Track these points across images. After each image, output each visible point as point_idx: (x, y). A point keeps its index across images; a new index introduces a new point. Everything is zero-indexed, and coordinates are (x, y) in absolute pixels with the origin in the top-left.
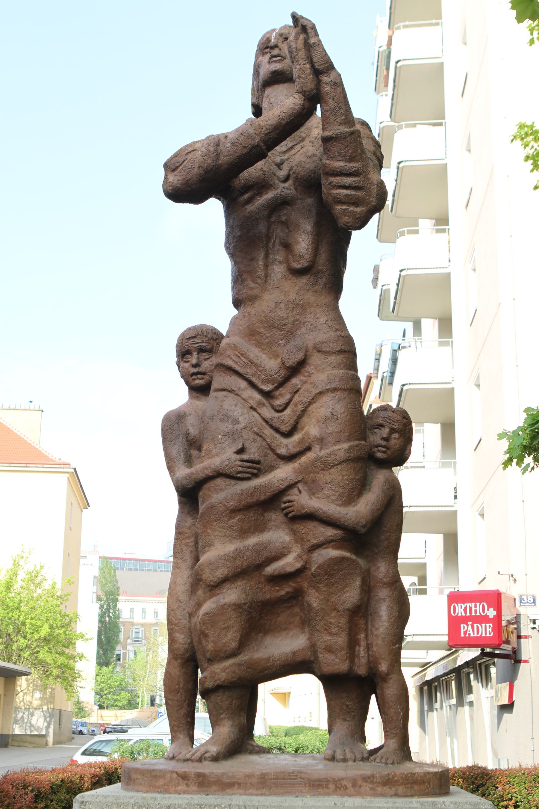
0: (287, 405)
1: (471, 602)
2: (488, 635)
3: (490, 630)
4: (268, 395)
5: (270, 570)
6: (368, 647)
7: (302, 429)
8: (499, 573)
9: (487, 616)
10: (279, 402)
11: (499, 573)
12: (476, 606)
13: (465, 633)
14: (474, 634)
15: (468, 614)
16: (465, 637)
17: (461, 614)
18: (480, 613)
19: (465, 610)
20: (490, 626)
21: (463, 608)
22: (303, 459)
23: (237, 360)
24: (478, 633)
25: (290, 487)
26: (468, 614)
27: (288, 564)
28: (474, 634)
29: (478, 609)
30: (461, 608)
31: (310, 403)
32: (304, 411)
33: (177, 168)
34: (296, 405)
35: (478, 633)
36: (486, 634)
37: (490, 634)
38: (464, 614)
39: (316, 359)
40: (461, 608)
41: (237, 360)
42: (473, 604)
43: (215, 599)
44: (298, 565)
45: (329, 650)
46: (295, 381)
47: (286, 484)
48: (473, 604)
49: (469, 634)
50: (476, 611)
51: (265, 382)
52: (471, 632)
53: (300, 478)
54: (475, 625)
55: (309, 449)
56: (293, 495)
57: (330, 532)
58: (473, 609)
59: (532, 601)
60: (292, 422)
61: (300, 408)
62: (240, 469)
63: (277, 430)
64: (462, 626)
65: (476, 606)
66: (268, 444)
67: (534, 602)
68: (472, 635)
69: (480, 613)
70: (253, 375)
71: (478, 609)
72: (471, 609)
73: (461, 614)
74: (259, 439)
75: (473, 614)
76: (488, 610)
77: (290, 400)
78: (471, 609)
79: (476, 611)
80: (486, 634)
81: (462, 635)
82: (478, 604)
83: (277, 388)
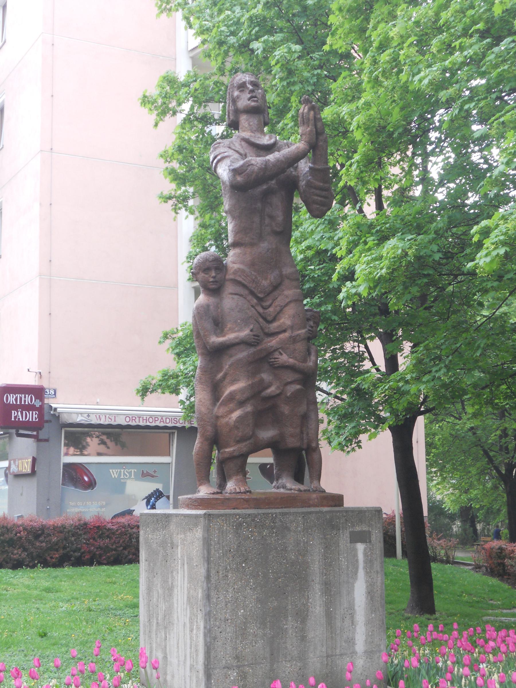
0: (270, 306)
1: (22, 394)
2: (34, 420)
3: (36, 416)
4: (260, 300)
5: (264, 394)
6: (308, 434)
7: (279, 320)
8: (29, 370)
9: (34, 406)
10: (265, 304)
11: (29, 370)
12: (25, 397)
13: (15, 417)
14: (22, 419)
15: (18, 403)
16: (15, 421)
17: (13, 402)
18: (28, 402)
19: (16, 400)
20: (36, 413)
21: (14, 398)
22: (282, 336)
23: (245, 278)
24: (26, 417)
25: (275, 351)
26: (18, 403)
27: (272, 391)
28: (22, 419)
29: (28, 399)
30: (13, 397)
31: (285, 306)
32: (281, 310)
33: (242, 173)
34: (276, 307)
35: (26, 417)
36: (32, 419)
37: (36, 419)
38: (15, 403)
39: (287, 282)
40: (13, 397)
41: (245, 278)
42: (23, 395)
43: (242, 409)
44: (278, 392)
45: (292, 436)
46: (275, 293)
47: (273, 349)
48: (23, 395)
49: (19, 419)
50: (25, 401)
51: (261, 292)
52: (20, 417)
53: (280, 346)
54: (24, 412)
55: (285, 331)
56: (276, 355)
57: (297, 376)
58: (23, 399)
59: (53, 393)
60: (274, 315)
61: (278, 309)
62: (254, 340)
63: (265, 319)
64: (13, 412)
65: (25, 397)
66: (261, 327)
67: (55, 394)
68: (21, 420)
69: (28, 402)
70: (254, 288)
71: (28, 399)
72: (21, 398)
73: (13, 402)
74: (257, 324)
75: (23, 403)
76: (35, 401)
77: (272, 303)
78: (21, 398)
79: (25, 401)
80: (32, 419)
81: (13, 419)
82: (27, 395)
83: (266, 296)
